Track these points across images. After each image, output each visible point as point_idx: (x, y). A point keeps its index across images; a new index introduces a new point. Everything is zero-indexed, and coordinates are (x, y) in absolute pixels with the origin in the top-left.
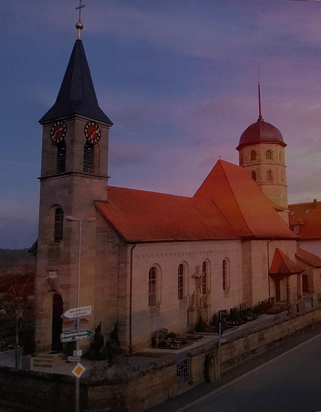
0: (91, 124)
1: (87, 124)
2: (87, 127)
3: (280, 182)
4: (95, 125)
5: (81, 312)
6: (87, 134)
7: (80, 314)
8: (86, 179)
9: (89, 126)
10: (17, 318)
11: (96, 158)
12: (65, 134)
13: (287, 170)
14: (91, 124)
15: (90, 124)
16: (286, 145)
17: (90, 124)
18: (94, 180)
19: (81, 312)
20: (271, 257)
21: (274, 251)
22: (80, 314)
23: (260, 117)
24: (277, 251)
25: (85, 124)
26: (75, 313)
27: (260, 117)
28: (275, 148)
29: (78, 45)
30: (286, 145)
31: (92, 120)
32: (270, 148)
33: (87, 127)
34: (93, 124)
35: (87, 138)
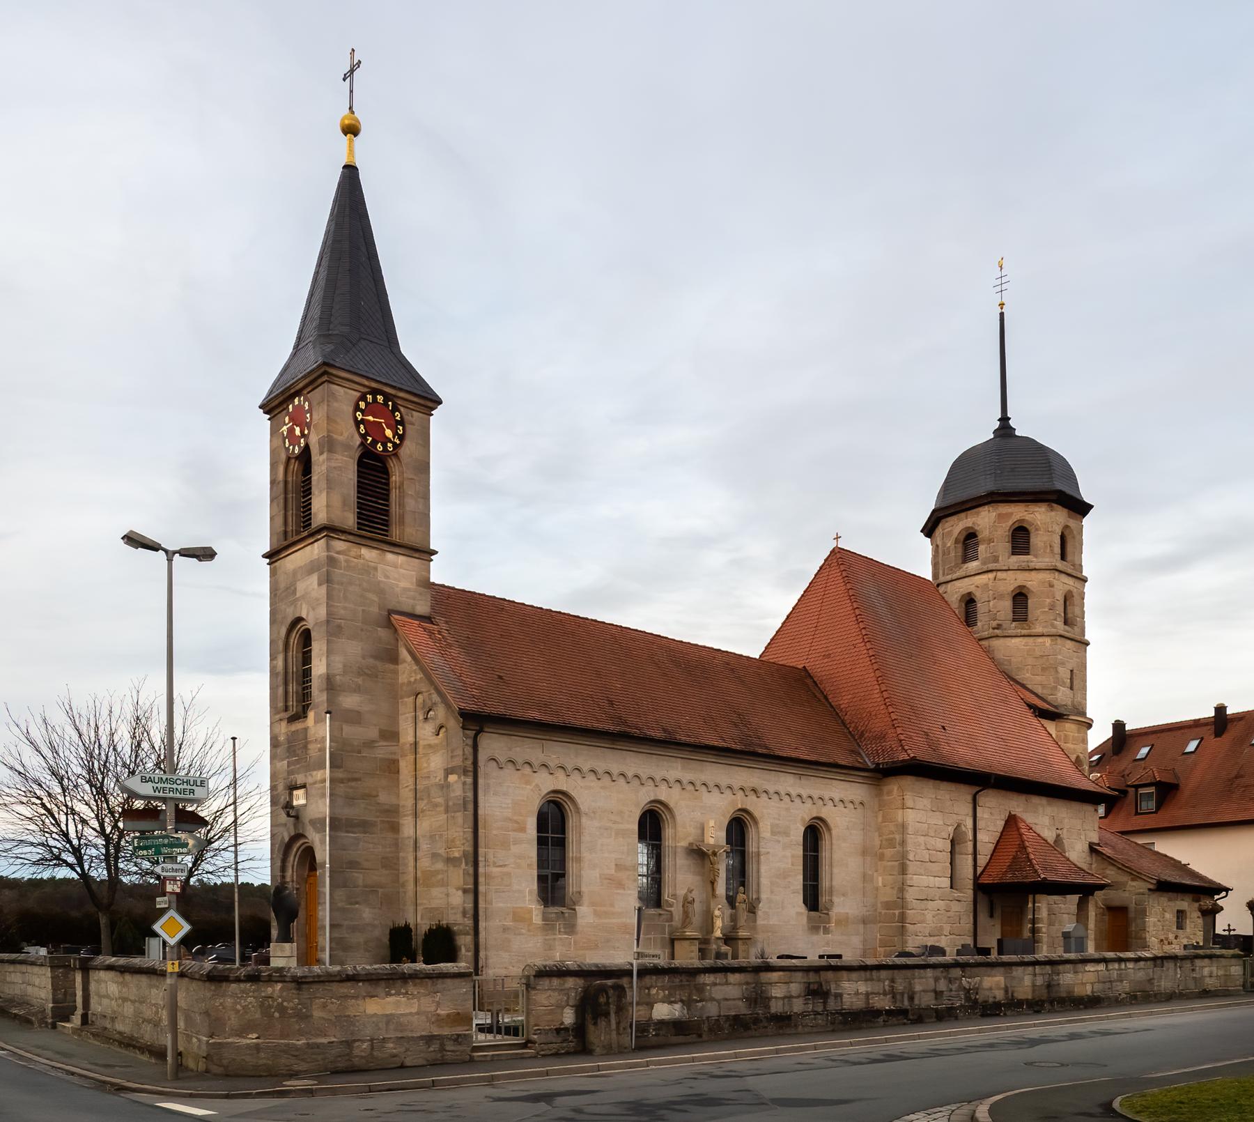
0: (375, 399)
1: (363, 398)
2: (362, 405)
3: (1060, 627)
4: (386, 401)
5: (175, 786)
6: (362, 427)
7: (171, 790)
8: (364, 551)
9: (367, 404)
10: (356, 1052)
11: (394, 495)
12: (309, 429)
13: (1088, 588)
14: (375, 399)
15: (369, 397)
16: (1091, 507)
17: (369, 397)
18: (390, 556)
19: (175, 786)
20: (987, 839)
21: (1003, 823)
22: (171, 790)
23: (1004, 419)
24: (1012, 822)
25: (355, 399)
26: (159, 785)
27: (1004, 419)
28: (1045, 520)
29: (350, 174)
30: (1091, 507)
31: (374, 385)
32: (1028, 517)
33: (362, 405)
34: (380, 398)
35: (364, 437)
